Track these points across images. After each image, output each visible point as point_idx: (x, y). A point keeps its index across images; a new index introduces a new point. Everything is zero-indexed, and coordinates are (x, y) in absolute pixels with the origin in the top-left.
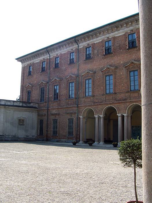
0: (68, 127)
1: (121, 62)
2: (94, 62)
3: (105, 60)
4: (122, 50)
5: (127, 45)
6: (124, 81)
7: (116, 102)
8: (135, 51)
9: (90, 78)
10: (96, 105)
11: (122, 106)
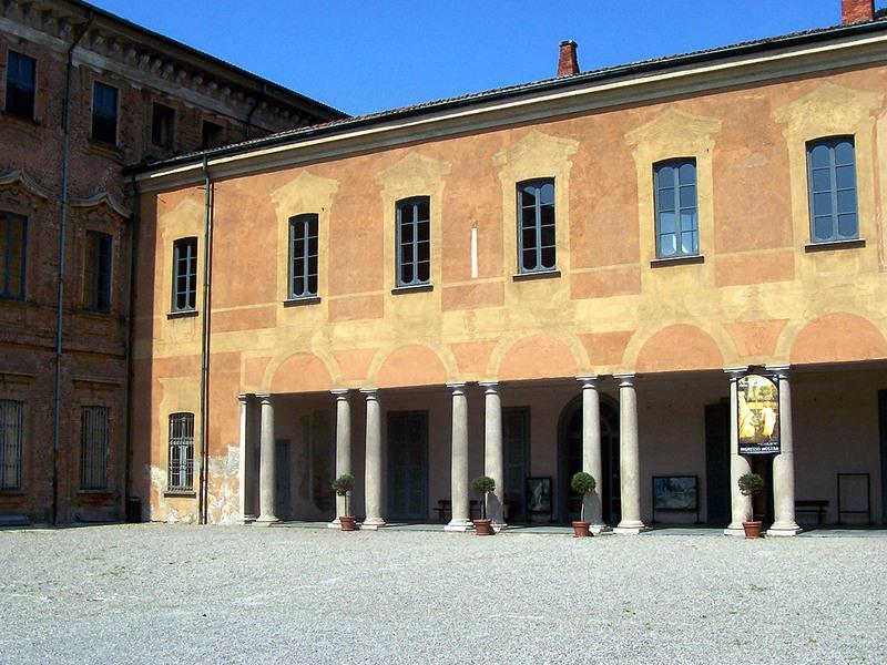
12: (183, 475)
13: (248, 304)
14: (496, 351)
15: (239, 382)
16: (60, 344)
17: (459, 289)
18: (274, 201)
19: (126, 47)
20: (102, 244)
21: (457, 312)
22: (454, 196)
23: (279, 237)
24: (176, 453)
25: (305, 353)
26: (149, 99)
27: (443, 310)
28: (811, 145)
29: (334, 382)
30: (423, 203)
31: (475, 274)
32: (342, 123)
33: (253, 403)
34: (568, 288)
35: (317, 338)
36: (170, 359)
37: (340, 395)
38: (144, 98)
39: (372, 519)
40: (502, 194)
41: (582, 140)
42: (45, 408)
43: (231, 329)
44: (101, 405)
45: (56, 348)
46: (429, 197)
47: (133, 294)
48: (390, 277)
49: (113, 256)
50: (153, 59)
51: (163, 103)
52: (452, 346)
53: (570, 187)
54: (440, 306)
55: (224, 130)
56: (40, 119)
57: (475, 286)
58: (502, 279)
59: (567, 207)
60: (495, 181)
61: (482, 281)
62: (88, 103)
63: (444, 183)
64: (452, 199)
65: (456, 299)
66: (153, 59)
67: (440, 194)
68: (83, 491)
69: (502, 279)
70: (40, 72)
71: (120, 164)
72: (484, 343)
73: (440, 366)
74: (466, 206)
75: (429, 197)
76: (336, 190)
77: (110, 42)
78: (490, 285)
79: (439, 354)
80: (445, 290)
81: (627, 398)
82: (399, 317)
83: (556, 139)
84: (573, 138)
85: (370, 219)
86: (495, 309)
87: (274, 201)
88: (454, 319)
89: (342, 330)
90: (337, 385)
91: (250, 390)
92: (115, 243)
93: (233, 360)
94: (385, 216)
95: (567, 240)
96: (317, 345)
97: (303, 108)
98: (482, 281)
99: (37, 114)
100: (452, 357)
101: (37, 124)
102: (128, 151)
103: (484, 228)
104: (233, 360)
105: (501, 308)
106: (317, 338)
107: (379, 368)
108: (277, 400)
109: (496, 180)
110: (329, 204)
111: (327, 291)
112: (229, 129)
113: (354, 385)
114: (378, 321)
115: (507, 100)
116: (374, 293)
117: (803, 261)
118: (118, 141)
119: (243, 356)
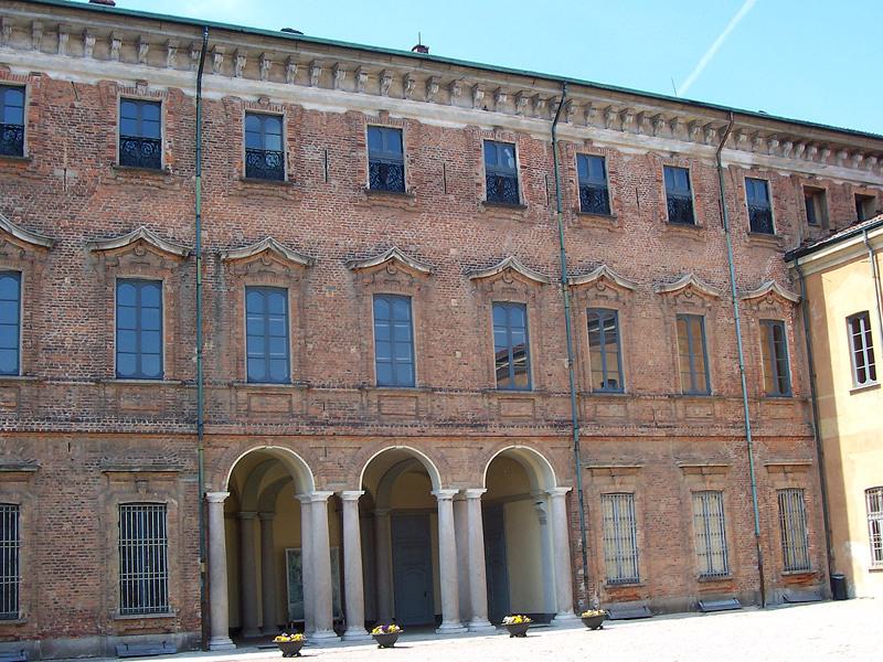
0: (117, 556)
1: (453, 251)
2: (304, 209)
3: (368, 215)
4: (452, 197)
5: (478, 185)
7: (439, 432)
10: (322, 437)
38: (794, 185)
42: (743, 495)
47: (813, 376)
92: (788, 328)
101: (699, 228)
102: (786, 237)
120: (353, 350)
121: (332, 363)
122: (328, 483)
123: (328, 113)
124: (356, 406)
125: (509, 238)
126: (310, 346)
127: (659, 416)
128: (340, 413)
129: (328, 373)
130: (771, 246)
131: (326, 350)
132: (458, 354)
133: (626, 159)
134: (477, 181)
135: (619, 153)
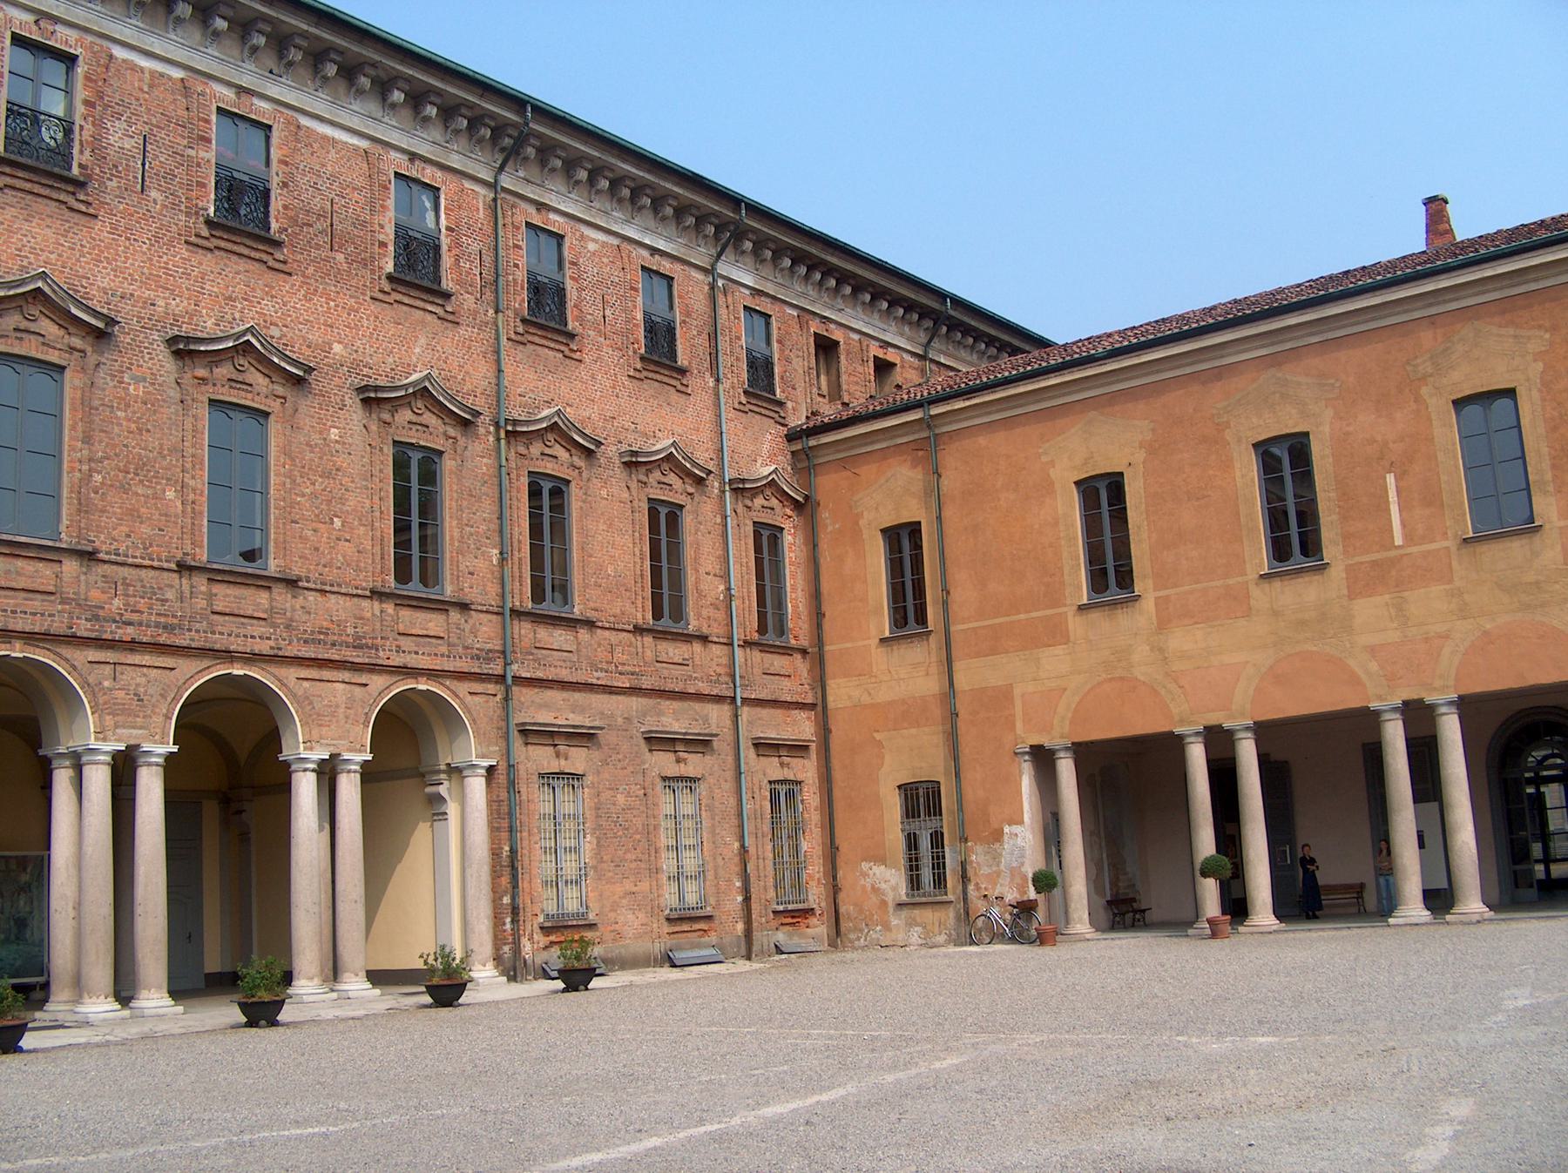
1: (337, 348)
3: (208, 262)
4: (340, 257)
6: (351, 503)
8: (429, 317)
9: (54, 357)
11: (336, 691)
12: (927, 874)
13: (1019, 613)
14: (1446, 651)
15: (1013, 728)
16: (738, 690)
17: (1374, 563)
18: (1044, 459)
19: (777, 255)
20: (767, 540)
21: (1377, 600)
22: (1351, 429)
23: (1060, 512)
24: (912, 842)
25: (1122, 679)
26: (808, 329)
27: (1351, 597)
28: (1459, 404)
29: (1177, 718)
30: (1299, 448)
31: (1398, 541)
32: (1036, 360)
33: (1043, 758)
34: (1559, 548)
35: (1141, 653)
36: (891, 703)
37: (1442, 705)
39: (1472, 903)
40: (1430, 419)
41: (1554, 329)
43: (993, 651)
44: (792, 778)
45: (734, 698)
46: (1307, 434)
48: (1258, 553)
49: (787, 560)
50: (810, 269)
51: (825, 334)
52: (1372, 650)
53: (1544, 400)
54: (1345, 592)
55: (898, 369)
56: (686, 363)
57: (1402, 556)
58: (1446, 544)
59: (1541, 430)
60: (1416, 401)
61: (1409, 550)
62: (739, 338)
63: (1329, 413)
64: (1347, 434)
65: (1364, 582)
66: (810, 269)
67: (1327, 429)
68: (781, 908)
69: (1446, 544)
70: (680, 297)
71: (783, 425)
72: (1427, 640)
73: (1355, 681)
74: (1372, 441)
75: (1307, 434)
76: (1149, 436)
77: (758, 247)
78: (1425, 555)
79: (1352, 663)
80: (1349, 569)
81: (1451, 731)
82: (1276, 613)
83: (1511, 331)
84: (1540, 327)
85: (1211, 472)
86: (1437, 590)
87: (1044, 459)
88: (1370, 611)
89: (1180, 640)
90: (1182, 722)
91: (1036, 740)
92: (788, 538)
93: (1001, 698)
94: (1237, 465)
95: (1549, 476)
96: (1142, 663)
97: (1006, 337)
98: (1414, 549)
99: (682, 360)
100: (1374, 666)
101: (683, 372)
103: (1405, 472)
104: (1001, 698)
105: (1447, 587)
106: (1141, 653)
107: (1251, 692)
108: (1084, 753)
109: (1418, 399)
110: (1140, 456)
111: (1150, 583)
112: (903, 367)
113: (1213, 719)
114: (1242, 622)
115: (1425, 281)
116: (1231, 582)
117: (1076, 625)
118: (778, 391)
119: (1017, 691)
120: (170, 494)
121: (133, 514)
122: (116, 727)
123: (152, 73)
124: (170, 595)
125: (422, 341)
126: (98, 478)
127: (619, 656)
128: (142, 604)
129: (125, 529)
130: (772, 414)
131: (125, 489)
132: (337, 522)
133: (592, 246)
134: (382, 237)
135: (582, 235)
